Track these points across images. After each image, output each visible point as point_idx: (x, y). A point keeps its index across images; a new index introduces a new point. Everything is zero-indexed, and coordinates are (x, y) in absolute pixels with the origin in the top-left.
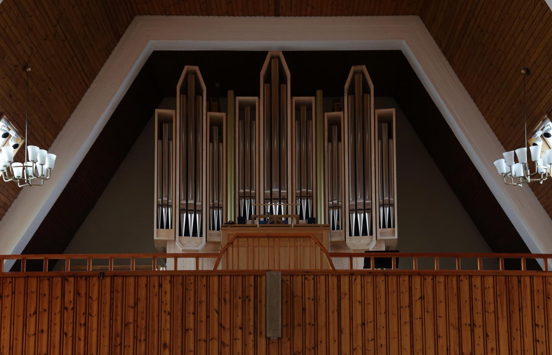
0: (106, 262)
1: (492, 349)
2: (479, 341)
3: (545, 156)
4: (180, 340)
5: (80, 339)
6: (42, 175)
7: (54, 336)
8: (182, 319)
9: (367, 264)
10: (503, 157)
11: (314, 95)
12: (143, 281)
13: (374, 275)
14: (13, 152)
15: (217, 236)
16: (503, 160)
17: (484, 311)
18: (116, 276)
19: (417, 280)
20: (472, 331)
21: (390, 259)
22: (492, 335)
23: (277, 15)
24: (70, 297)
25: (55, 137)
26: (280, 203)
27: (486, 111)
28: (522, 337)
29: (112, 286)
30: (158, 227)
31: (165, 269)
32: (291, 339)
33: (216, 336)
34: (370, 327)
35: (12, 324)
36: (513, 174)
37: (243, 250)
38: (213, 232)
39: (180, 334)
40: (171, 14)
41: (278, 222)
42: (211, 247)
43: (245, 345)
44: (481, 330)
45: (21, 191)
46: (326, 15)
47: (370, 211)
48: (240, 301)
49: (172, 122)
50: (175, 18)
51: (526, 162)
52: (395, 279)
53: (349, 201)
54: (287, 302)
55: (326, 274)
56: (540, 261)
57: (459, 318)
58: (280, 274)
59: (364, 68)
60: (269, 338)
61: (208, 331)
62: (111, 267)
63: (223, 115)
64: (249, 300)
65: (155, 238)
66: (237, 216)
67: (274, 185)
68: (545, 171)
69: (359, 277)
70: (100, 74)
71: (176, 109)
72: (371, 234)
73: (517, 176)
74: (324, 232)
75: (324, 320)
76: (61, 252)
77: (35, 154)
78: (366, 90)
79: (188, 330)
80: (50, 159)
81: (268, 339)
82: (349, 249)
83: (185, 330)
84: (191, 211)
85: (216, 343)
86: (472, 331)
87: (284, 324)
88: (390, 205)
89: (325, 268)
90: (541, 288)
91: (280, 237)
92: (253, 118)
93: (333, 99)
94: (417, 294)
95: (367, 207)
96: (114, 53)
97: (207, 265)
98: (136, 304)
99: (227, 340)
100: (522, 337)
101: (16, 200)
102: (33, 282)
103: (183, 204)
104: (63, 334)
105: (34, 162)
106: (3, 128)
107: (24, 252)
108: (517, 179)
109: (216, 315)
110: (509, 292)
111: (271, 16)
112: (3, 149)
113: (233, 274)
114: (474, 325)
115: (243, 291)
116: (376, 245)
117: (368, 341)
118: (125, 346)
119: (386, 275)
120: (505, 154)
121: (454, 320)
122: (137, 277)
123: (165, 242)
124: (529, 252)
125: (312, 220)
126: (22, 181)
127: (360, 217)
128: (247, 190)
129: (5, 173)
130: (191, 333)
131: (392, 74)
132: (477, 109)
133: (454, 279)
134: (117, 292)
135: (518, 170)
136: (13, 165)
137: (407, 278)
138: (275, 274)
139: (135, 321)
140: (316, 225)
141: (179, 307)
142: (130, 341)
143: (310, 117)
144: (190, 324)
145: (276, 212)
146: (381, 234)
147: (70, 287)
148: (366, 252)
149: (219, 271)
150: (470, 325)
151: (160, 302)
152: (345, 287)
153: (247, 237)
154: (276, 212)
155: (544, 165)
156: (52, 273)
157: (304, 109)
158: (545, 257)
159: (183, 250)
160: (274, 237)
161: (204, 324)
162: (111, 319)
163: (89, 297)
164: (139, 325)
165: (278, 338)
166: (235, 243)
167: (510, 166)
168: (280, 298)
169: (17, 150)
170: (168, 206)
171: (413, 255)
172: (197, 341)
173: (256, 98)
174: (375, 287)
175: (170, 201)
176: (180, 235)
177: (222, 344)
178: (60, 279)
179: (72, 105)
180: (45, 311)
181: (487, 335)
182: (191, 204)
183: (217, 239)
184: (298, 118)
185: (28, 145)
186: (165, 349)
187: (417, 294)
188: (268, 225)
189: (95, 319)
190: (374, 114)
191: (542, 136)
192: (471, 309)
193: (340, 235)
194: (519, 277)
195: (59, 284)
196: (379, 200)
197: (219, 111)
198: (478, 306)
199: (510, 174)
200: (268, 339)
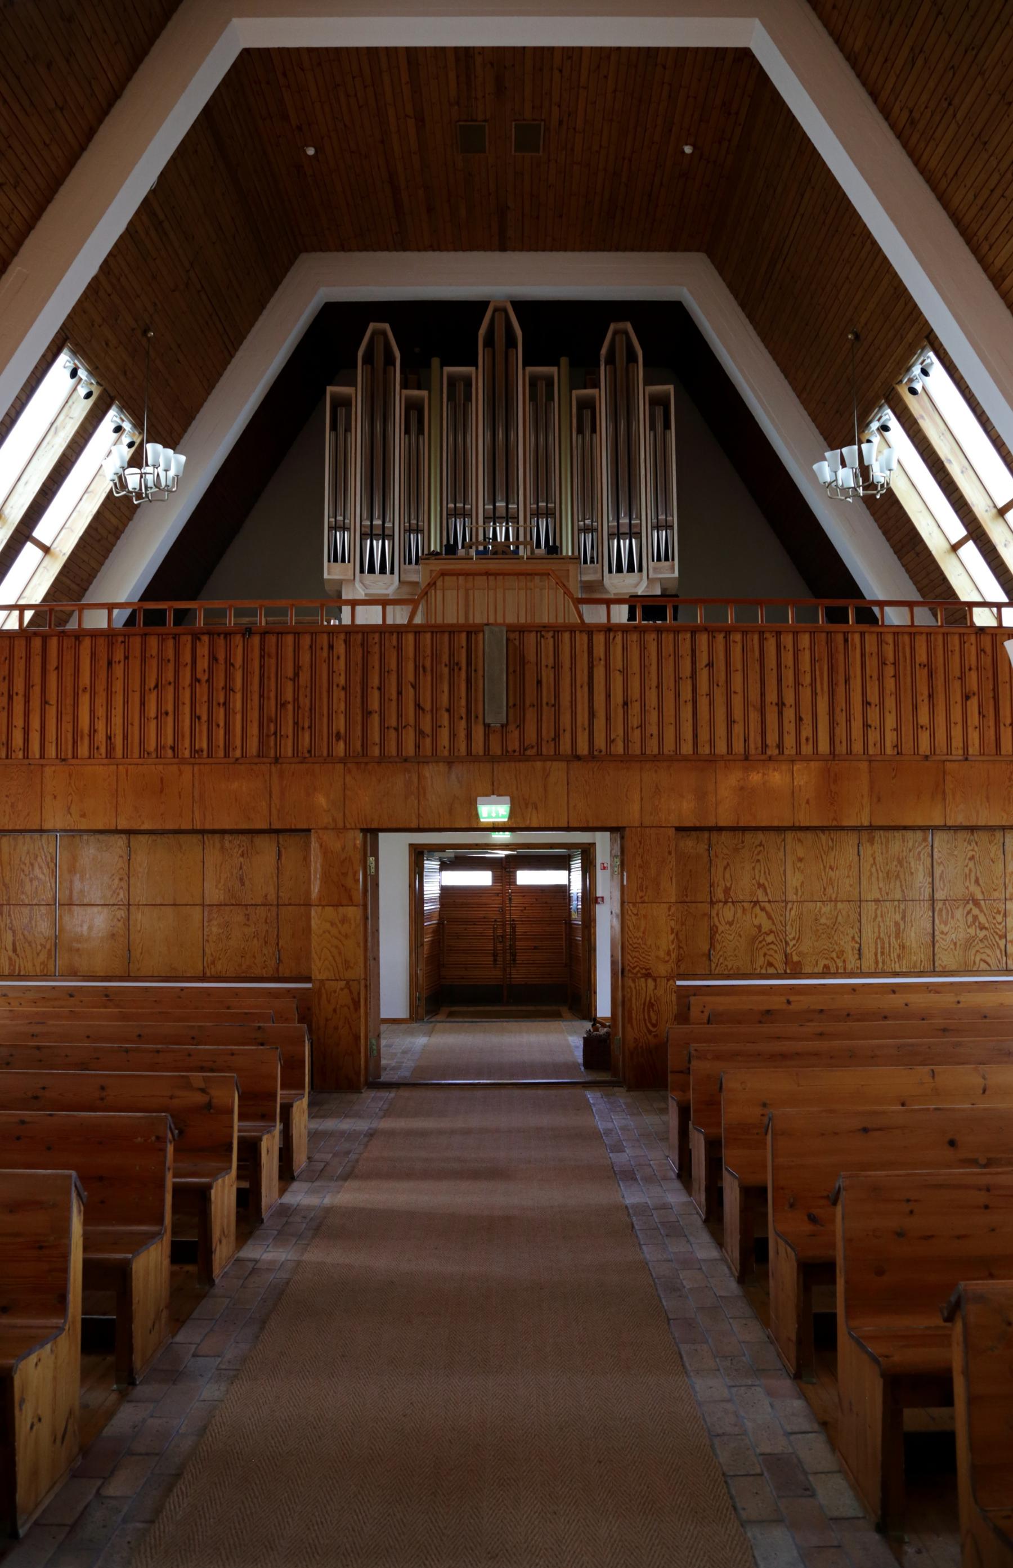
0: (252, 613)
1: (807, 739)
2: (790, 727)
3: (882, 458)
4: (359, 728)
5: (218, 726)
6: (167, 486)
7: (183, 721)
8: (363, 697)
9: (632, 617)
10: (824, 459)
11: (557, 364)
12: (306, 641)
13: (641, 631)
14: (127, 453)
15: (416, 574)
16: (826, 463)
17: (797, 683)
18: (267, 633)
19: (703, 639)
20: (780, 713)
21: (845, 610)
22: (807, 718)
23: (503, 248)
24: (203, 664)
25: (185, 431)
26: (507, 523)
27: (803, 391)
28: (848, 721)
29: (262, 649)
30: (329, 561)
31: (337, 623)
32: (521, 727)
33: (412, 721)
34: (635, 708)
35: (126, 702)
36: (840, 483)
37: (451, 595)
38: (410, 567)
39: (359, 718)
40: (350, 250)
41: (504, 553)
42: (406, 589)
43: (453, 735)
44: (792, 711)
45: (139, 510)
46: (573, 250)
47: (638, 535)
48: (446, 670)
49: (351, 405)
50: (357, 255)
51: (857, 465)
52: (671, 636)
53: (607, 522)
54: (514, 671)
55: (572, 630)
56: (876, 610)
57: (763, 694)
58: (504, 629)
59: (628, 326)
60: (489, 726)
61: (399, 715)
62: (262, 621)
63: (424, 393)
64: (460, 669)
65: (326, 576)
66: (445, 542)
67: (499, 497)
68: (882, 480)
69: (620, 634)
70: (250, 337)
71: (355, 385)
72: (640, 570)
73: (845, 486)
74: (571, 568)
75: (568, 698)
76: (193, 598)
77: (156, 456)
78: (632, 357)
79: (370, 713)
80: (178, 462)
81: (487, 726)
82: (607, 592)
83: (367, 714)
84: (377, 537)
85: (411, 732)
86: (780, 713)
87: (511, 704)
88: (668, 527)
89: (572, 621)
90: (875, 649)
91: (504, 574)
92: (468, 398)
93: (584, 372)
94: (703, 659)
95: (634, 530)
96: (269, 306)
97: (398, 616)
98: (296, 675)
99: (427, 728)
100: (848, 721)
101: (131, 523)
102: (153, 642)
103: (366, 526)
104: (195, 717)
105: (156, 466)
106: (115, 419)
107: (144, 598)
108: (844, 490)
109: (411, 691)
110: (831, 656)
111: (495, 250)
112: (114, 449)
113: (436, 630)
114: (783, 704)
115: (451, 655)
116: (647, 587)
117: (632, 728)
118: (281, 736)
119: (659, 631)
120: (827, 454)
121: (754, 696)
122: (297, 634)
123: (340, 583)
124: (861, 596)
125: (553, 550)
126: (139, 496)
127: (624, 544)
128: (460, 505)
129: (115, 484)
130: (376, 718)
131: (668, 335)
132: (789, 388)
133: (756, 637)
134: (269, 656)
135: (846, 477)
136: (127, 471)
137: (688, 636)
138: (496, 629)
139: (296, 699)
140: (559, 556)
141: (358, 679)
142: (288, 729)
143: (550, 397)
144: (375, 705)
145: (501, 537)
146: (655, 569)
147: (203, 650)
148: (631, 596)
149: (417, 625)
150: (777, 704)
151: (331, 672)
152: (599, 650)
153: (457, 574)
154: (501, 537)
155: (882, 471)
156: (179, 629)
157: (542, 386)
158: (882, 604)
159: (366, 595)
160: (496, 575)
161: (394, 704)
162: (261, 696)
163: (230, 665)
164: (301, 705)
165: (502, 726)
166: (439, 583)
167: (836, 472)
168: (505, 667)
169: (133, 449)
170: (344, 528)
171: (728, 602)
172: (383, 728)
173: (473, 369)
174: (643, 648)
175: (347, 521)
176: (362, 571)
177: (420, 733)
178: (189, 638)
179: (209, 383)
180: (170, 683)
181: (801, 719)
182: (378, 525)
183: (414, 578)
184: (533, 397)
185: (147, 442)
186: (337, 740)
187: (703, 659)
188: (489, 556)
189: (239, 696)
190: (643, 393)
191: (878, 429)
192: (779, 680)
193: (595, 572)
194: (845, 634)
195: (189, 646)
196: (652, 519)
197: (419, 388)
198: (789, 676)
199: (834, 484)
200: (487, 726)
